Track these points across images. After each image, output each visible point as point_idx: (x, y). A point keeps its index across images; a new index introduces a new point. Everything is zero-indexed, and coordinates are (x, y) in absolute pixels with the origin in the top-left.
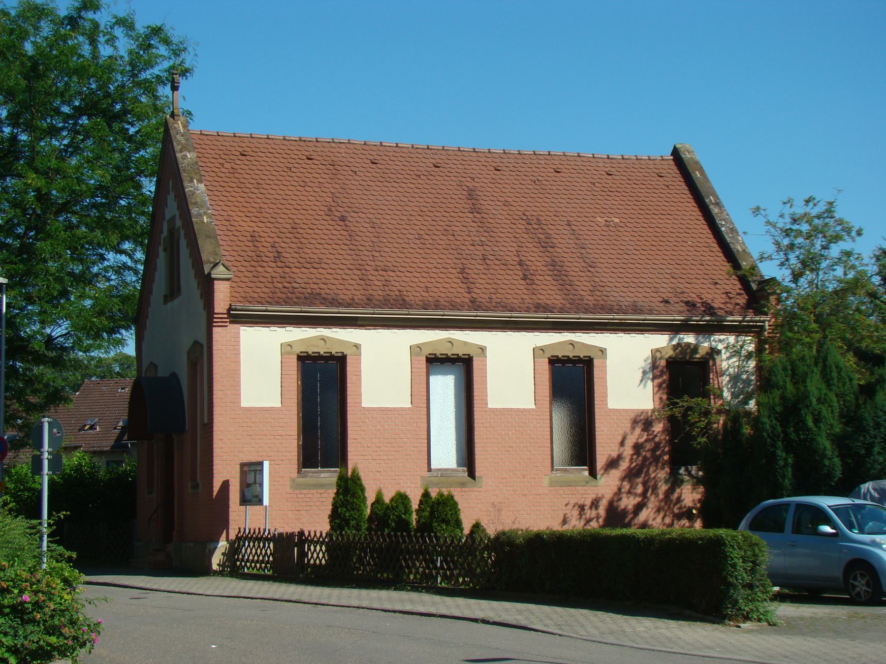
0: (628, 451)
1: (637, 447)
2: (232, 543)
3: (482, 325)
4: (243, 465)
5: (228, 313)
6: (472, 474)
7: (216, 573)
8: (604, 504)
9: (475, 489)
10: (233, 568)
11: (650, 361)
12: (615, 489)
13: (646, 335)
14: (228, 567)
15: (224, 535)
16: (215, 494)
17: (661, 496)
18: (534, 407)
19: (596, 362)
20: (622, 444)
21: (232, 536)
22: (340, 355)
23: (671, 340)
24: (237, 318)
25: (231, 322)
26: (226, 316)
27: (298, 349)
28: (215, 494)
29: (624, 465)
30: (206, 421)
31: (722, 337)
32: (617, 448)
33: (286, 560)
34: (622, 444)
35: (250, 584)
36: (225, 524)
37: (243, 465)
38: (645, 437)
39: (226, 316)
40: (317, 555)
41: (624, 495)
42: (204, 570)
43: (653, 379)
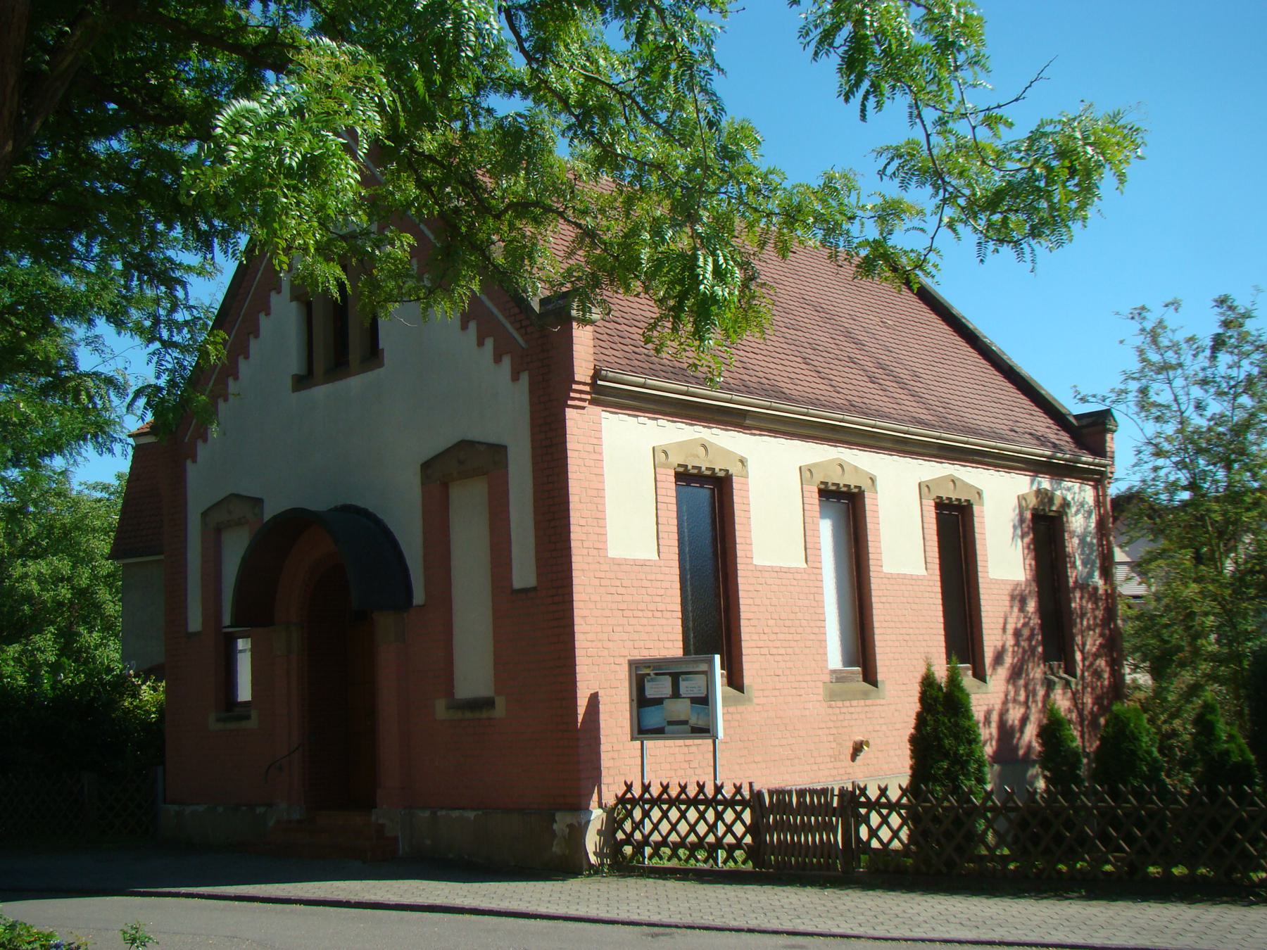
0: (1010, 641)
1: (1017, 634)
2: (610, 812)
3: (951, 455)
4: (634, 665)
5: (593, 384)
6: (870, 676)
7: (595, 871)
8: (995, 717)
9: (878, 701)
10: (622, 862)
11: (1017, 511)
12: (1002, 696)
13: (855, 452)
14: (606, 856)
15: (595, 796)
16: (580, 718)
17: (1040, 705)
18: (924, 572)
19: (975, 508)
20: (1004, 629)
21: (609, 800)
22: (722, 474)
23: (1032, 482)
24: (607, 395)
25: (593, 402)
26: (587, 388)
27: (676, 459)
28: (580, 718)
29: (1008, 660)
30: (524, 574)
31: (1070, 484)
32: (999, 637)
33: (796, 842)
34: (1004, 629)
35: (672, 887)
36: (595, 776)
37: (634, 665)
38: (1022, 621)
39: (587, 388)
40: (888, 832)
41: (1010, 705)
42: (568, 866)
43: (1022, 537)
